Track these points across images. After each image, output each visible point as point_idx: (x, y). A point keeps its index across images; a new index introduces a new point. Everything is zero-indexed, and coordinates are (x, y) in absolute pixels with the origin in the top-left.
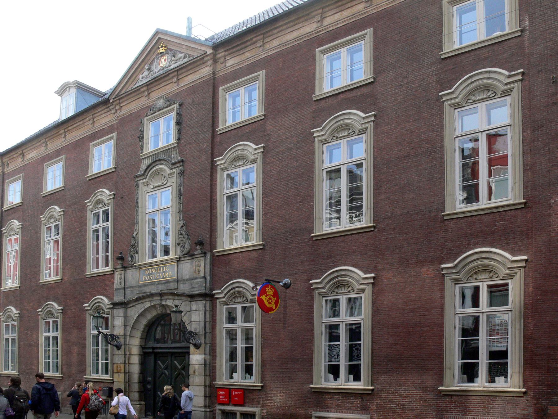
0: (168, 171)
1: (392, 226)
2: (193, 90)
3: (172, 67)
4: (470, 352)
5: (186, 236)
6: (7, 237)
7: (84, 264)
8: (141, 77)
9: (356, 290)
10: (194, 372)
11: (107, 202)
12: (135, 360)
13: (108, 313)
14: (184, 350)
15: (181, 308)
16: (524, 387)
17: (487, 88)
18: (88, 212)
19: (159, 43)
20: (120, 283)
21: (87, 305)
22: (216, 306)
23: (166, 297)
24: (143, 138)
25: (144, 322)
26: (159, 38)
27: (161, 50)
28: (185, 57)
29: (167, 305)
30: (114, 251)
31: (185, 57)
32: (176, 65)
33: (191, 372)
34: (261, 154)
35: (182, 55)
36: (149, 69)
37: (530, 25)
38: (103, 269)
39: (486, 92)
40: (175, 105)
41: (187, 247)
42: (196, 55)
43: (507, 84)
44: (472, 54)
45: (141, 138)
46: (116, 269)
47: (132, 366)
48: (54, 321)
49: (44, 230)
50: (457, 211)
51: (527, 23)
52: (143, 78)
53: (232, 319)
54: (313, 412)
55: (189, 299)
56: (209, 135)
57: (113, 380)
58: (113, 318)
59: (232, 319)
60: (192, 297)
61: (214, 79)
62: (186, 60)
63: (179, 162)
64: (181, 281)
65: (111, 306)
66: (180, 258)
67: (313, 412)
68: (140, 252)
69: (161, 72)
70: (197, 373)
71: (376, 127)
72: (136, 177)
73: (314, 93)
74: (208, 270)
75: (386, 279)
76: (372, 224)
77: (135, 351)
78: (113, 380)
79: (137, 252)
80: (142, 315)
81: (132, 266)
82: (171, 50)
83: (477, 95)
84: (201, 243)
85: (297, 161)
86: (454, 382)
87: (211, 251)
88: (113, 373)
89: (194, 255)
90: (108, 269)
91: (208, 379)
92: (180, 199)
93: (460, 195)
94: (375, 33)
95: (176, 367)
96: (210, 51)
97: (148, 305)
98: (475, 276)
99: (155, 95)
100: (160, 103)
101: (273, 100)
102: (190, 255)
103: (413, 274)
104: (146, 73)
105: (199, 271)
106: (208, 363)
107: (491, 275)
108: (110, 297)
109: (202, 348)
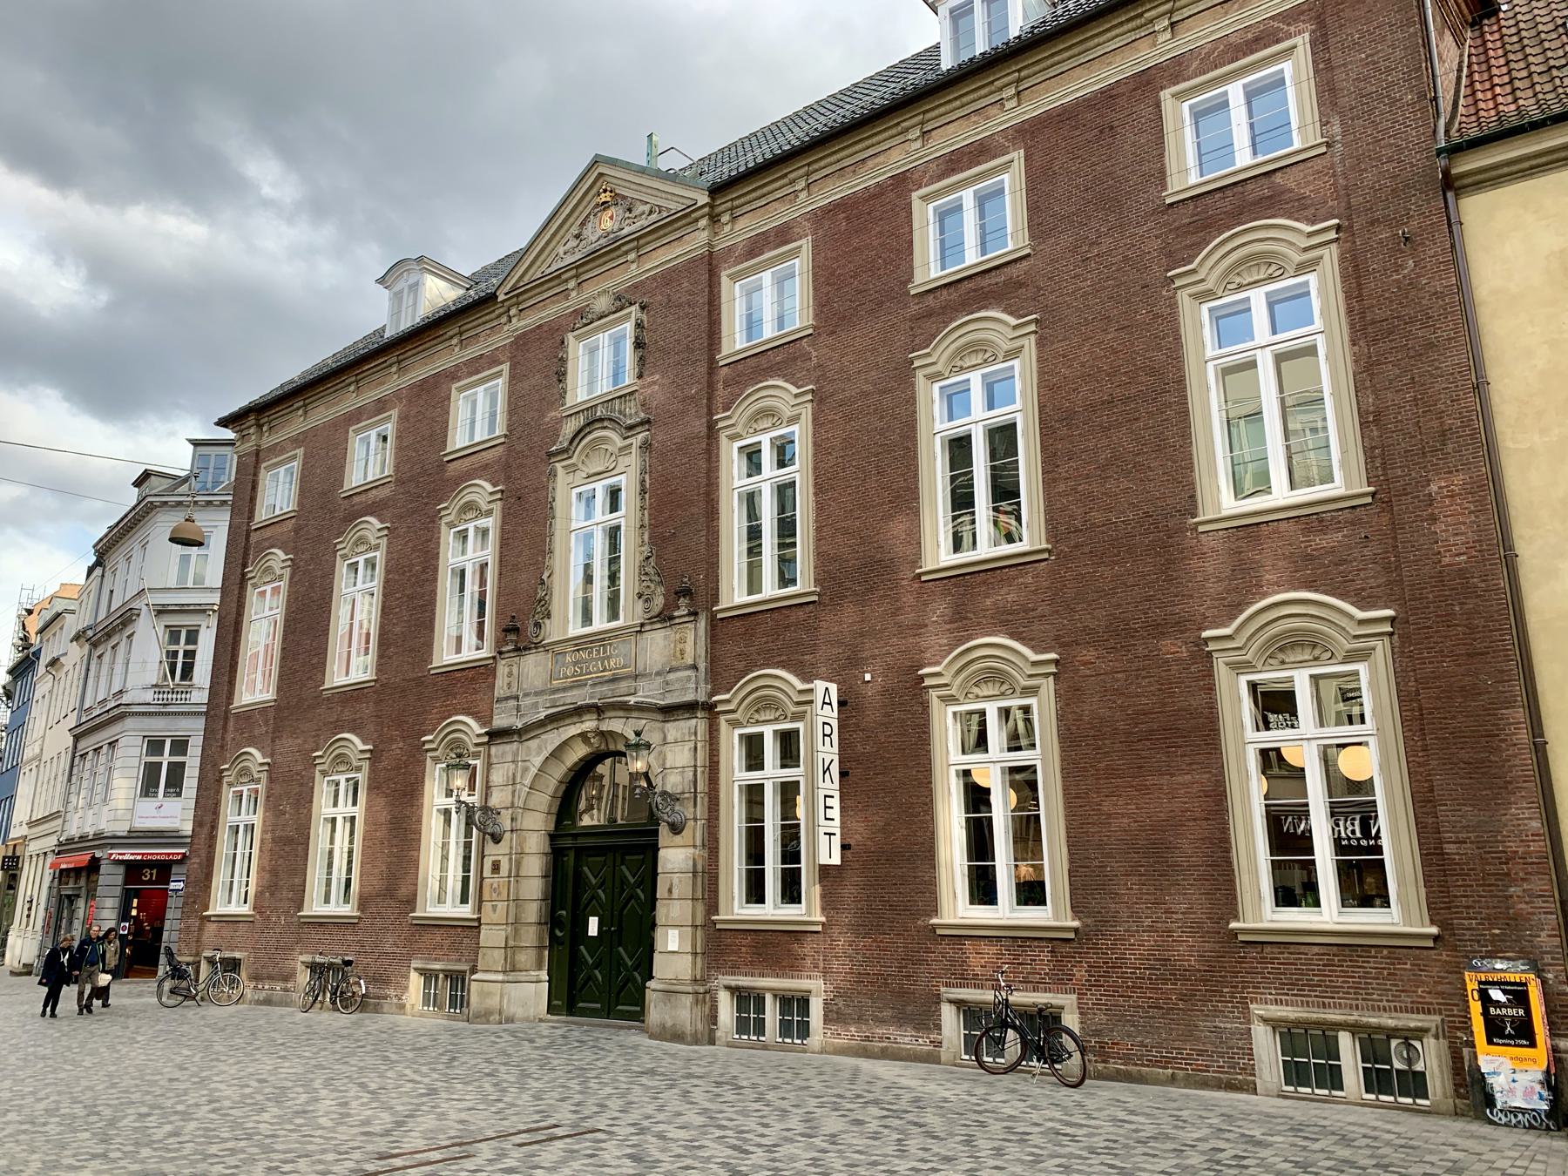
0: (620, 443)
1: (1087, 549)
2: (668, 278)
3: (626, 231)
4: (1288, 838)
5: (657, 578)
6: (255, 586)
7: (429, 645)
8: (561, 250)
9: (1018, 690)
10: (670, 891)
11: (485, 507)
12: (534, 866)
13: (476, 755)
14: (643, 840)
15: (645, 737)
16: (1433, 922)
17: (1265, 259)
18: (444, 528)
19: (598, 183)
20: (509, 685)
21: (430, 738)
22: (718, 730)
23: (609, 714)
24: (565, 374)
25: (559, 771)
26: (601, 175)
27: (604, 197)
28: (651, 212)
29: (611, 733)
30: (499, 613)
31: (651, 212)
32: (633, 228)
33: (661, 892)
34: (809, 406)
35: (647, 208)
36: (577, 236)
37: (1344, 133)
38: (469, 653)
39: (1263, 268)
40: (633, 308)
41: (659, 602)
42: (674, 207)
43: (1306, 250)
44: (1229, 193)
45: (561, 376)
46: (500, 653)
47: (524, 883)
48: (348, 780)
49: (342, 569)
50: (1225, 513)
51: (1337, 129)
52: (566, 254)
53: (754, 759)
54: (943, 989)
55: (660, 717)
56: (702, 369)
57: (479, 919)
58: (489, 766)
59: (754, 759)
60: (669, 712)
61: (711, 253)
62: (654, 217)
63: (642, 423)
64: (644, 675)
65: (486, 739)
66: (642, 625)
67: (943, 989)
68: (554, 613)
69: (603, 242)
70: (676, 894)
71: (1041, 344)
72: (551, 455)
73: (910, 279)
74: (702, 651)
75: (1085, 664)
76: (1044, 546)
77: (536, 844)
78: (479, 919)
79: (549, 616)
80: (556, 754)
81: (537, 646)
82: (624, 198)
83: (1245, 274)
84: (686, 592)
85: (882, 418)
86: (1262, 912)
87: (709, 609)
88: (481, 901)
89: (674, 618)
90: (483, 653)
91: (700, 908)
92: (643, 499)
93: (946, 541)
94: (1028, 158)
95: (624, 881)
96: (703, 199)
97: (574, 730)
98: (1281, 656)
99: (590, 289)
100: (602, 304)
101: (830, 289)
102: (665, 617)
103: (1141, 650)
104: (573, 243)
105: (682, 652)
106: (700, 868)
107: (1317, 652)
108: (484, 719)
109: (687, 832)
